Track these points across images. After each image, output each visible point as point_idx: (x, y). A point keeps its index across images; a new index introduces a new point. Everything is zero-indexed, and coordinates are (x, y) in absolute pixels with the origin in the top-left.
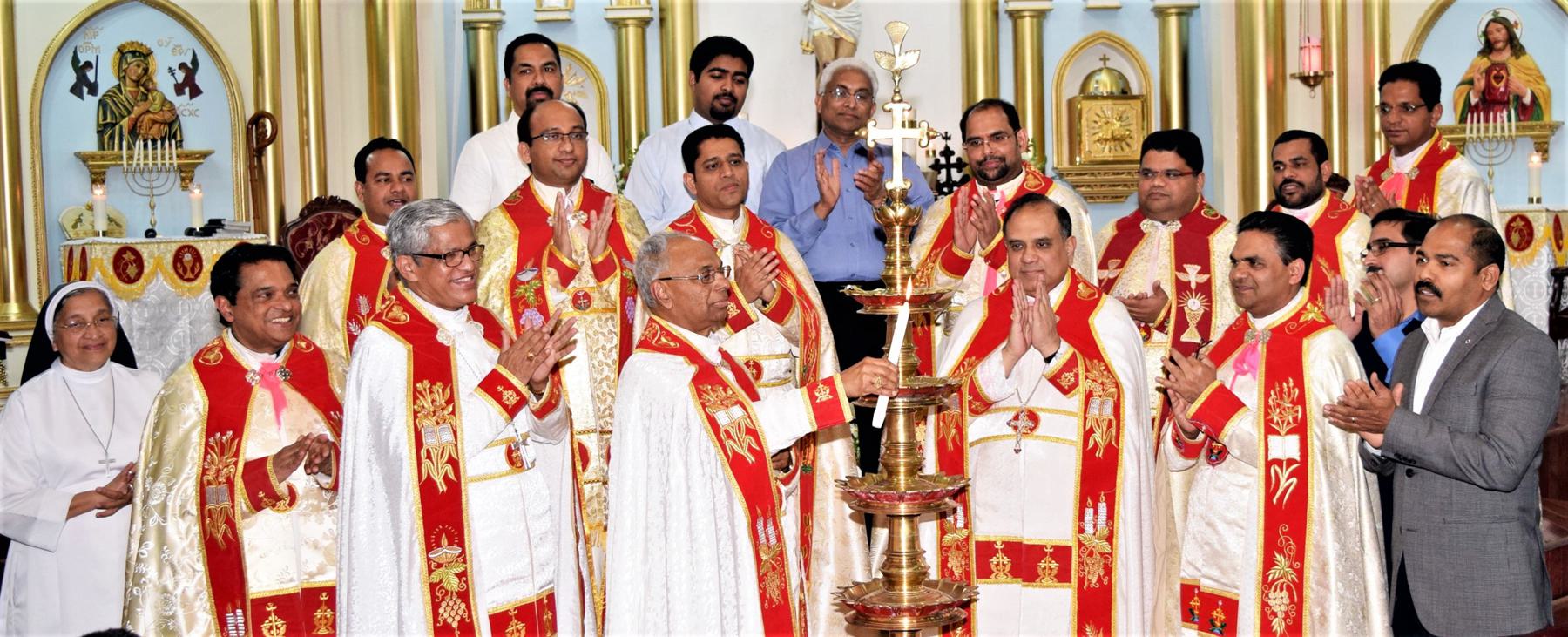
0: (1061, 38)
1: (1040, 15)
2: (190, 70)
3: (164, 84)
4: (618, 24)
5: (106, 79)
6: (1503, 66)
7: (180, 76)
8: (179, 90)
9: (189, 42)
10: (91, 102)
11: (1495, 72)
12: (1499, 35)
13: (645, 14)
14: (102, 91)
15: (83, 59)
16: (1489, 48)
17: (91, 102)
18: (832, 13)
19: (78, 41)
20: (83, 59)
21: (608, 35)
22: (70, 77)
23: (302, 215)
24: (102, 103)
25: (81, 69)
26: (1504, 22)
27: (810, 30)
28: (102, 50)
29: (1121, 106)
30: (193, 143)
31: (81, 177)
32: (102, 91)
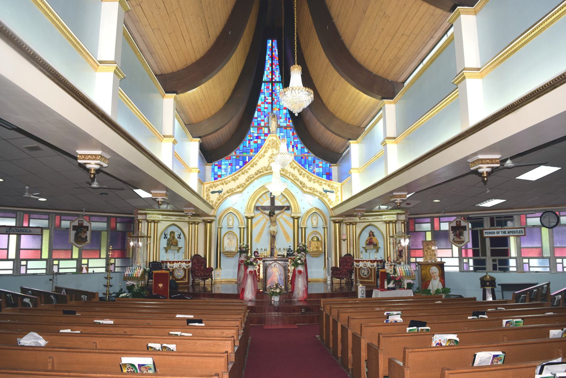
0: (308, 232)
1: (305, 228)
2: (180, 235)
3: (176, 237)
4: (240, 228)
5: (168, 237)
6: (372, 238)
7: (178, 236)
8: (178, 238)
9: (180, 231)
10: (166, 240)
11: (371, 239)
12: (371, 234)
13: (244, 227)
14: (168, 238)
15: (166, 233)
16: (370, 236)
17: (166, 240)
18: (273, 227)
19: (165, 231)
20: (166, 233)
21: (238, 230)
22: (164, 236)
23: (345, 256)
24: (168, 240)
25: (165, 235)
26: (372, 232)
27: (408, 367)
28: (168, 232)
29: (318, 242)
30: (180, 246)
31: (164, 251)
32: (168, 238)
